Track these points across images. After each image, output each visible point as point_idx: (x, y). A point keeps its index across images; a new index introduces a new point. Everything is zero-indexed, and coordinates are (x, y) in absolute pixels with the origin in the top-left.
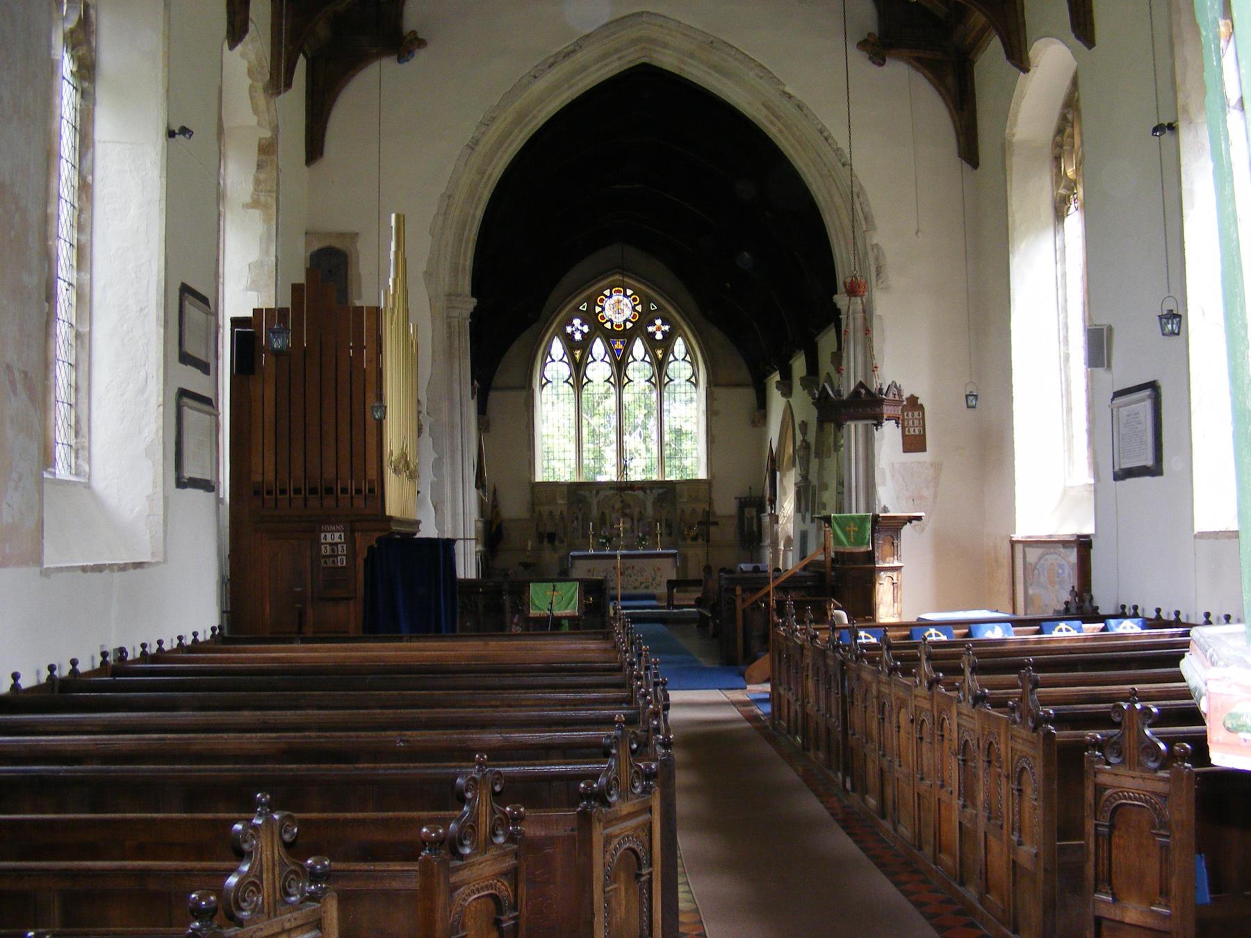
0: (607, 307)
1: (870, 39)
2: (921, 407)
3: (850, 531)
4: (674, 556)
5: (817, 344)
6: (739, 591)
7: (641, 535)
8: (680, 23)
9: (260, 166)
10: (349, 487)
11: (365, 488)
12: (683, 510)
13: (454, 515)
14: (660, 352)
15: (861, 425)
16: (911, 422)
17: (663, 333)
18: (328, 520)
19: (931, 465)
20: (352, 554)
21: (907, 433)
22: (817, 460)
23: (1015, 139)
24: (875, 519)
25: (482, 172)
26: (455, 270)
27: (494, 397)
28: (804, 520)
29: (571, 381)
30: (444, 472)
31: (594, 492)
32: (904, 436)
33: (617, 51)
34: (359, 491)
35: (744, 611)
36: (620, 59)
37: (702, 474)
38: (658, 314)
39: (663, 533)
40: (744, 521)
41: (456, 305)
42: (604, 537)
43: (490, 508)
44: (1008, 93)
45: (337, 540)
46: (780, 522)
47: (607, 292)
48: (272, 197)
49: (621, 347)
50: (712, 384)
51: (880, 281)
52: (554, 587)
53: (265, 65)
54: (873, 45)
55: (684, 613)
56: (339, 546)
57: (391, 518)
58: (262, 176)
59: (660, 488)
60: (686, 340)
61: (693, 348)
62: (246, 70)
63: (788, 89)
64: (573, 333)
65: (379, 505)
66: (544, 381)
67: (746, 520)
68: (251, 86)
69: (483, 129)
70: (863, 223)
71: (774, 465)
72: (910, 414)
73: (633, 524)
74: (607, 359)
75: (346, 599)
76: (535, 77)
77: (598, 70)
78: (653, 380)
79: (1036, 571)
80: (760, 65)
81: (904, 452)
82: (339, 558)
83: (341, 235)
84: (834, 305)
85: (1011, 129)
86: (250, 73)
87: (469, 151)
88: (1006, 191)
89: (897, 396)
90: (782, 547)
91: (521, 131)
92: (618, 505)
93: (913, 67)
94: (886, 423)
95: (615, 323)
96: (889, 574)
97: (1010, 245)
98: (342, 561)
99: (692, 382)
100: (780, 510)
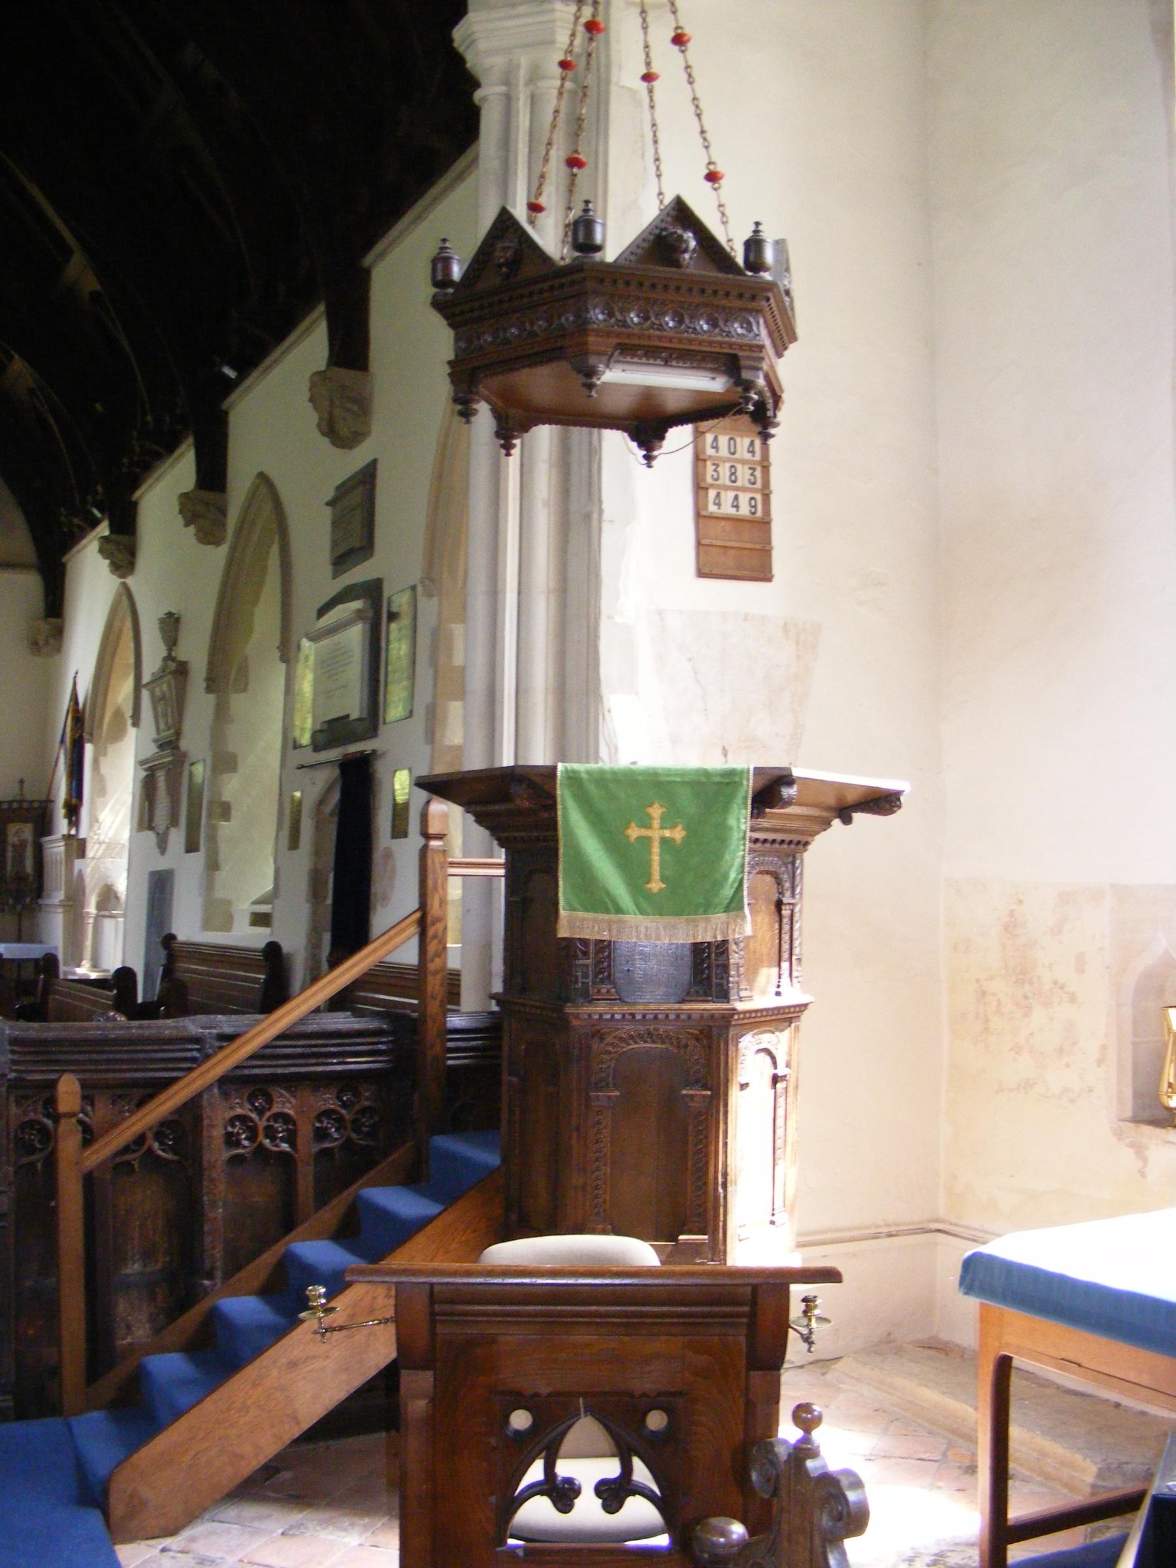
3: (646, 841)
6: (68, 1090)
19: (786, 628)
22: (211, 698)
28: (162, 846)
35: (89, 1181)
67: (10, 849)
72: (723, 440)
81: (701, 574)
90: (91, 908)
96: (767, 1039)
100: (91, 826)
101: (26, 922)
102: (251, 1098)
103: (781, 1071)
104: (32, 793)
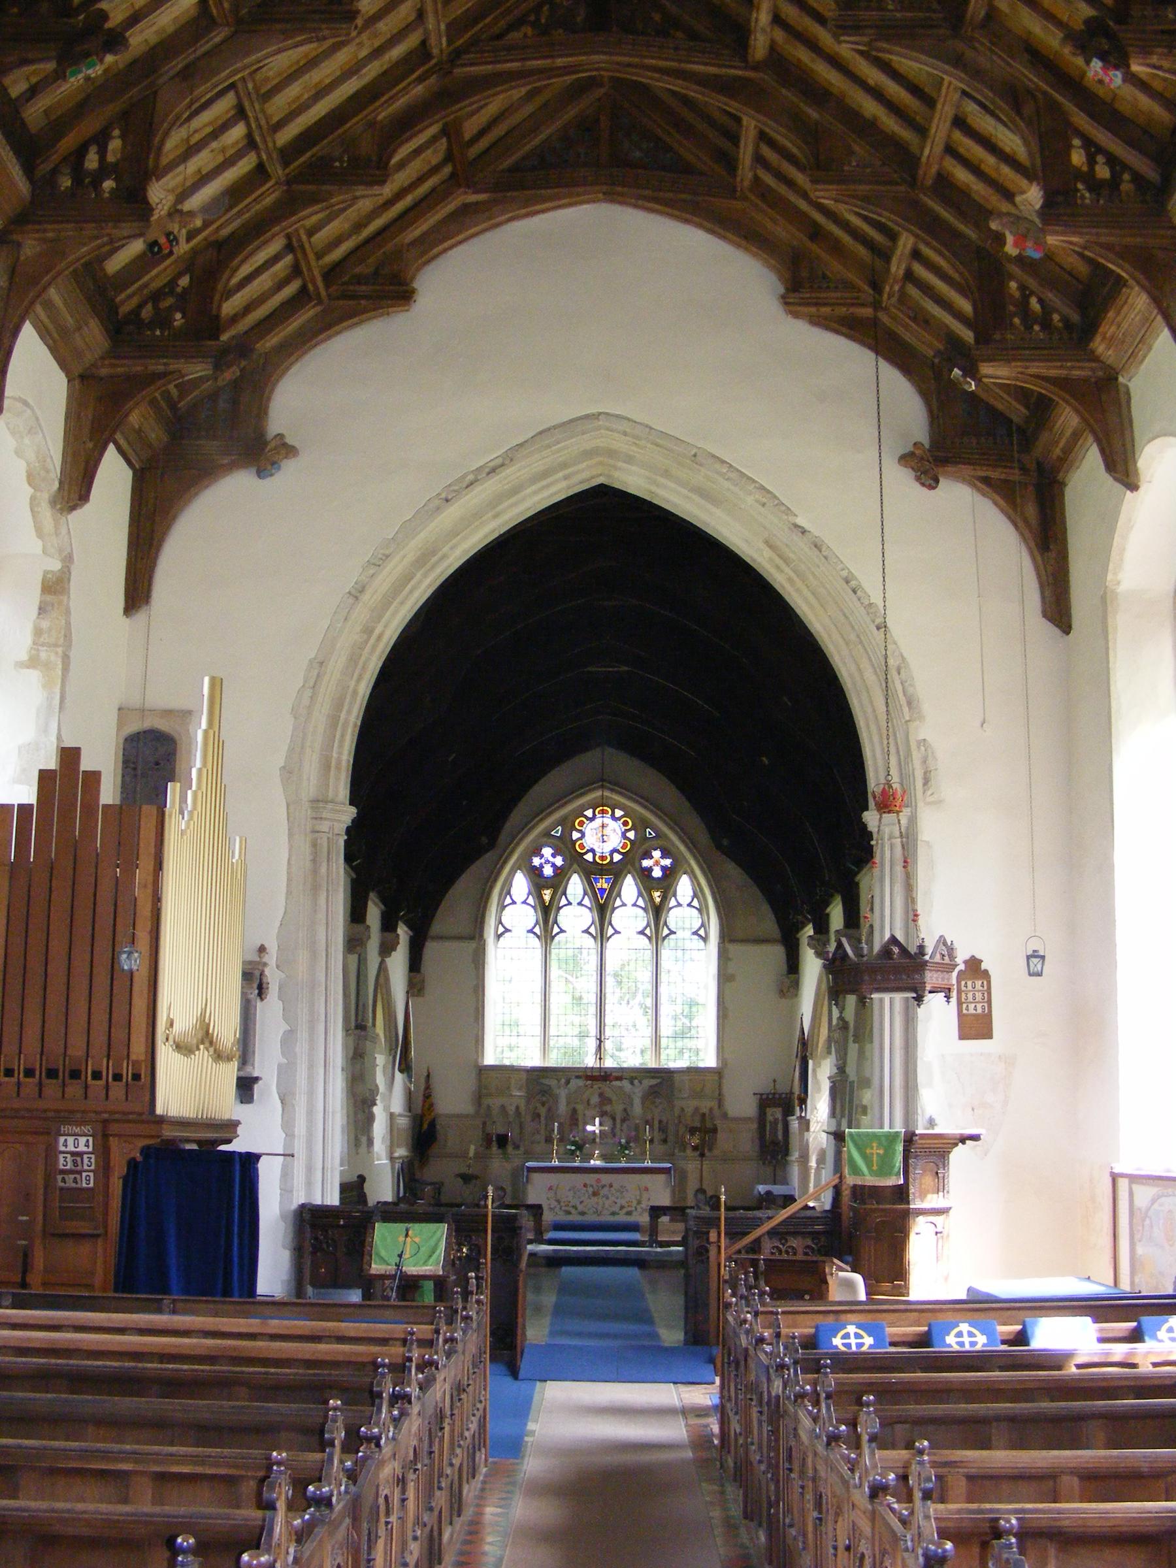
0: (588, 832)
1: (917, 452)
2: (986, 975)
4: (666, 1171)
5: (857, 884)
7: (623, 1141)
8: (651, 428)
9: (42, 610)
10: (38, 1066)
11: (127, 1071)
12: (683, 1110)
13: (310, 1113)
14: (658, 894)
15: (899, 997)
16: (970, 995)
17: (664, 869)
18: (67, 1118)
20: (104, 1168)
21: (965, 1011)
23: (1122, 588)
24: (910, 1139)
25: (368, 631)
26: (326, 766)
27: (432, 949)
29: (537, 930)
30: (297, 1049)
31: (563, 1081)
32: (960, 1015)
33: (564, 466)
34: (117, 1077)
36: (566, 478)
37: (709, 1059)
38: (655, 843)
39: (655, 1140)
40: (765, 1126)
41: (324, 815)
42: (574, 1143)
43: (421, 1098)
44: (1109, 520)
45: (82, 1148)
46: (812, 1129)
47: (589, 813)
48: (57, 653)
49: (605, 886)
50: (727, 937)
51: (929, 792)
52: (407, 1230)
53: (51, 467)
54: (922, 459)
55: (670, 1252)
56: (85, 1156)
57: (162, 1120)
58: (45, 624)
59: (653, 1078)
60: (693, 877)
61: (701, 890)
62: (24, 474)
63: (800, 521)
64: (542, 866)
65: (147, 1098)
66: (501, 930)
68: (33, 499)
69: (371, 572)
70: (906, 709)
71: (804, 1052)
72: (970, 983)
73: (614, 1124)
74: (586, 901)
75: (93, 1236)
76: (447, 500)
77: (535, 493)
78: (648, 932)
79: (1147, 1222)
80: (762, 488)
82: (84, 1174)
83: (168, 713)
84: (864, 826)
85: (1115, 574)
86: (31, 478)
87: (351, 600)
88: (1108, 662)
89: (946, 958)
90: (813, 1163)
91: (425, 576)
92: (595, 1100)
93: (979, 490)
94: (929, 997)
95: (598, 855)
97: (1114, 741)
98: (88, 1181)
99: (700, 936)
101: (779, 1173)
102: (780, 1240)
103: (939, 1230)
104: (782, 1088)
